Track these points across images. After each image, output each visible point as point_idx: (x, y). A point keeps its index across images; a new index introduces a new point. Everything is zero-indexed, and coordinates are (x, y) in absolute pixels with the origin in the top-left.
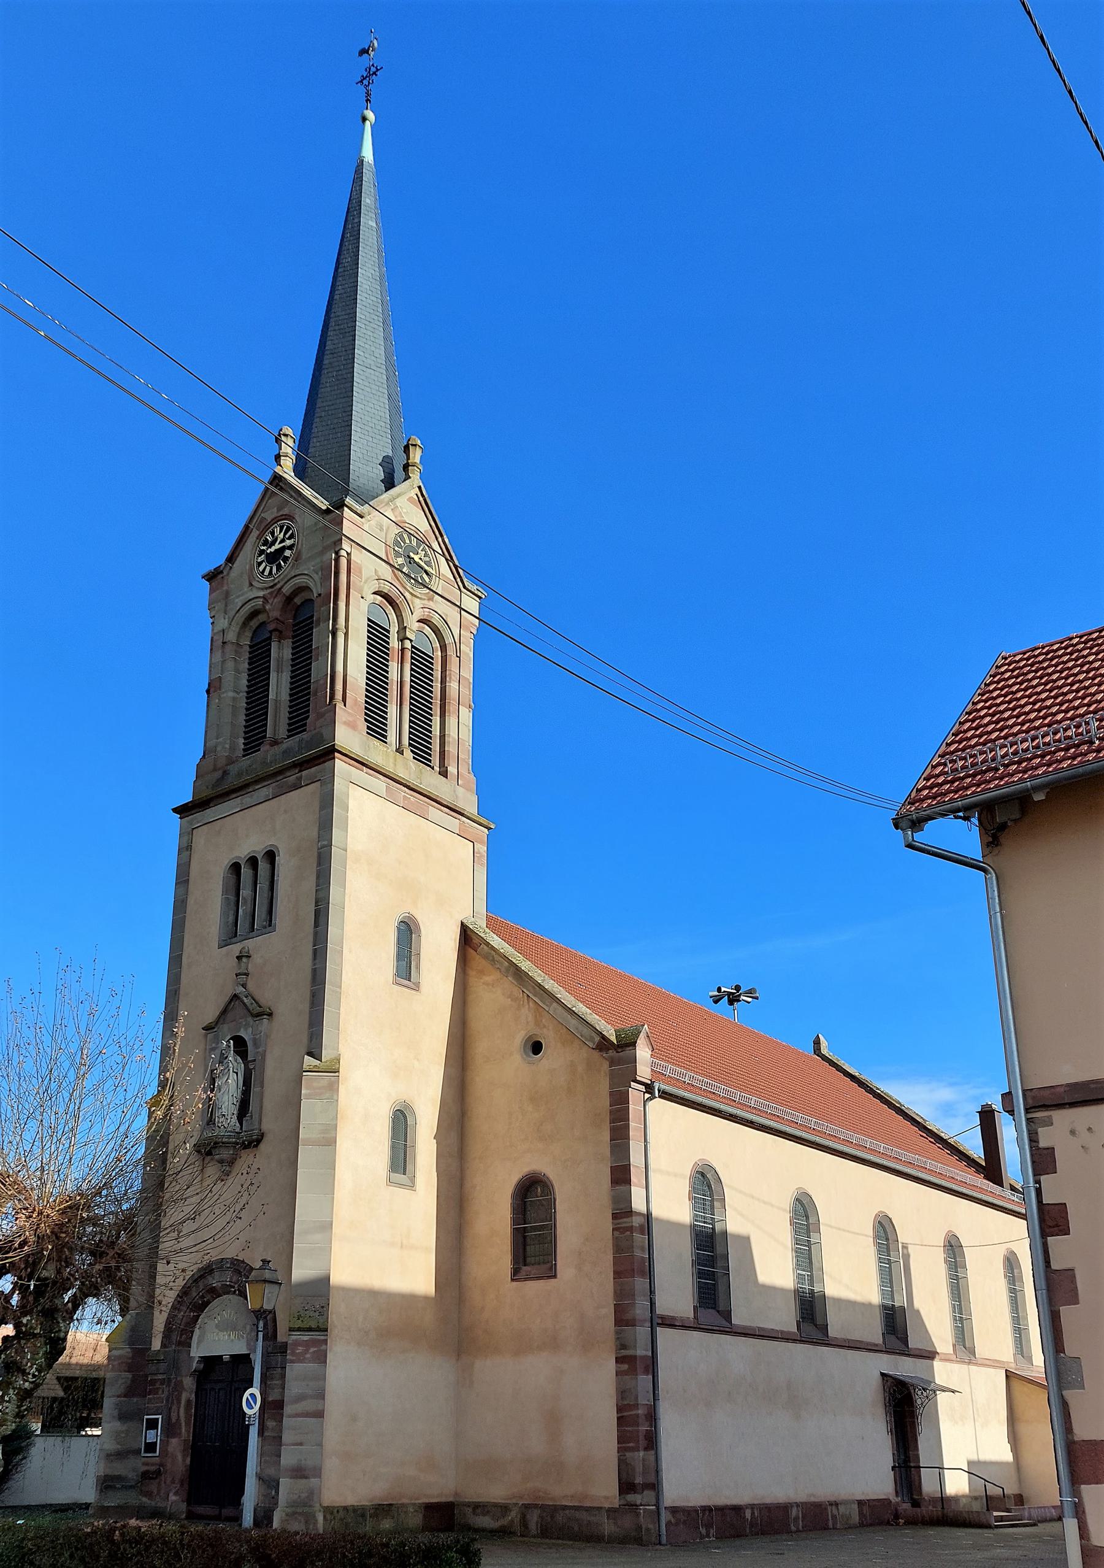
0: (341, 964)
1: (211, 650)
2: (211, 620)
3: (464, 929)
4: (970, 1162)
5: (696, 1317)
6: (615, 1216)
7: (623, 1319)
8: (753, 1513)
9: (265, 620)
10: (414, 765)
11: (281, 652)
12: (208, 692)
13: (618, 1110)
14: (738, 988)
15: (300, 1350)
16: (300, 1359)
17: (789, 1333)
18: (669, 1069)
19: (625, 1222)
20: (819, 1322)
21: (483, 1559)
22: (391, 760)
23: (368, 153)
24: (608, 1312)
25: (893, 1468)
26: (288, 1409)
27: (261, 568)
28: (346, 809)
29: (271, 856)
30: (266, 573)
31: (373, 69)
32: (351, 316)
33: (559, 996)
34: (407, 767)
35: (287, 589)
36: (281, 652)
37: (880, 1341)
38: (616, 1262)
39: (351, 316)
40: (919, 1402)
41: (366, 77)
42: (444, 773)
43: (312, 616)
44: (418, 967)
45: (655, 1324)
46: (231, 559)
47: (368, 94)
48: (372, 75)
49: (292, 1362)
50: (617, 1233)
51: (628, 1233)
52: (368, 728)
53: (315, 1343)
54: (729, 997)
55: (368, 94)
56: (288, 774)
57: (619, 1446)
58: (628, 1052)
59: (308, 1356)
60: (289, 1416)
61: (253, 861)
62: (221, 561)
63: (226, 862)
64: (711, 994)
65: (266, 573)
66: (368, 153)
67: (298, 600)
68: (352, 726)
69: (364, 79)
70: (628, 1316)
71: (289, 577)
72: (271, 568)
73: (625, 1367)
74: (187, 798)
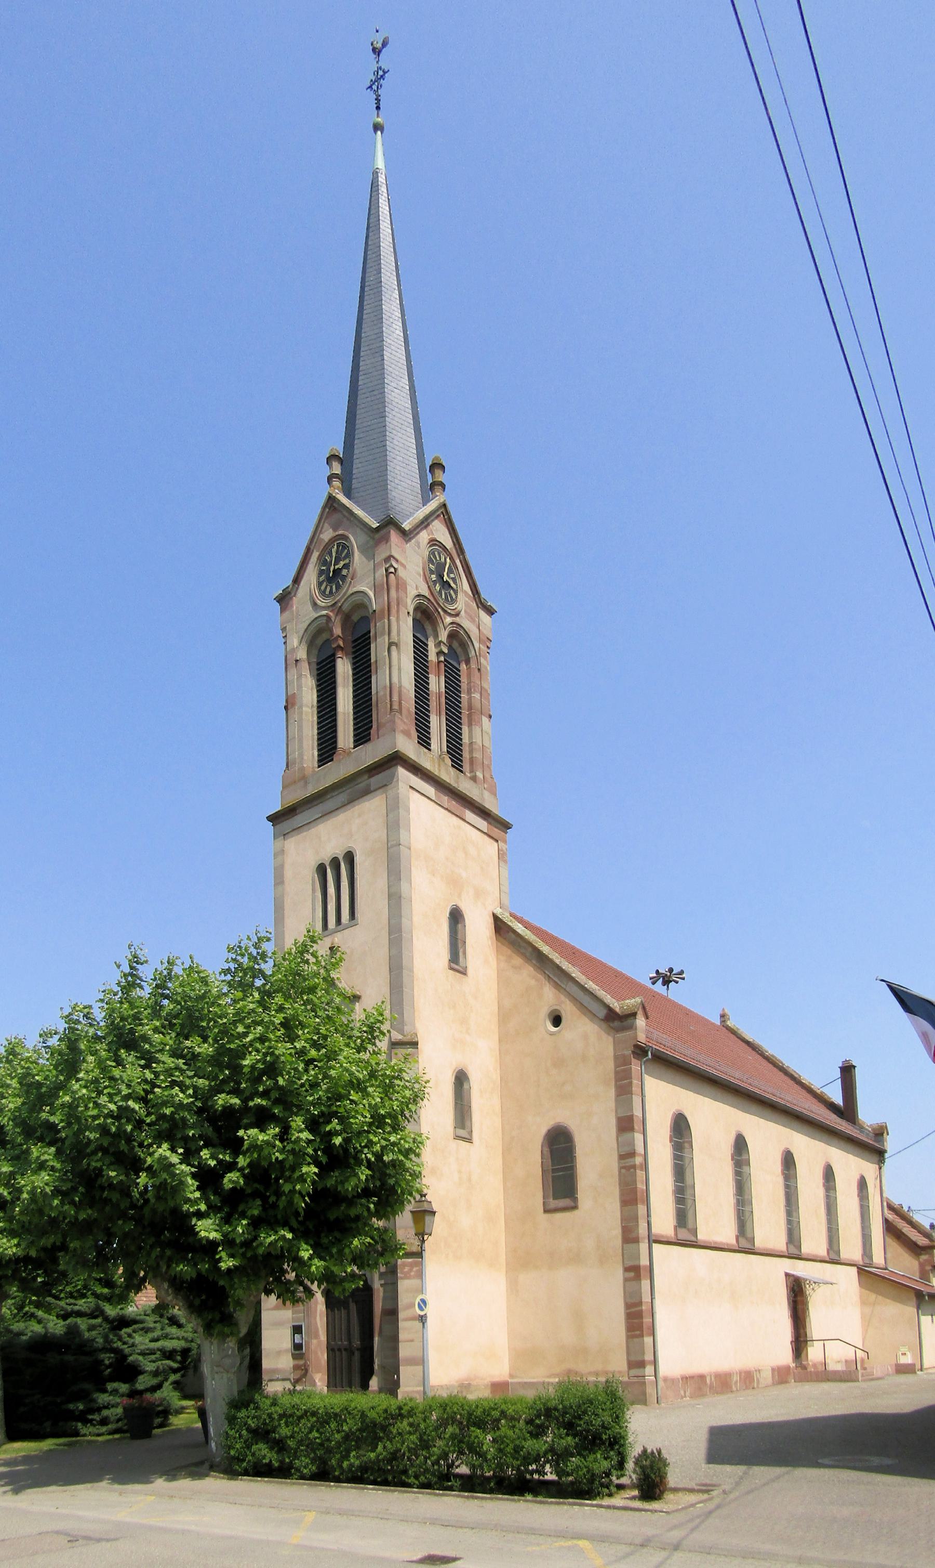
0: (412, 951)
1: (286, 668)
2: (284, 640)
3: (496, 918)
4: (832, 1107)
5: (676, 1234)
6: (622, 1157)
7: (629, 1237)
8: (711, 1379)
9: (329, 637)
10: (453, 771)
11: (344, 668)
12: (286, 708)
13: (624, 1071)
14: (671, 970)
15: (406, 1269)
16: (407, 1277)
17: (879, 1264)
18: (656, 1034)
19: (629, 1162)
20: (749, 1235)
21: (464, 1394)
22: (437, 766)
23: (380, 163)
24: (617, 1232)
25: (791, 1342)
26: (401, 1315)
27: (323, 588)
28: (408, 811)
29: (350, 857)
30: (327, 592)
31: (381, 73)
32: (378, 335)
33: (573, 975)
34: (447, 774)
35: (346, 607)
36: (344, 668)
37: (734, 1242)
38: (622, 1194)
39: (378, 335)
40: (808, 1293)
41: (375, 81)
42: (474, 779)
43: (369, 632)
44: (465, 953)
45: (651, 1241)
46: (297, 580)
47: (378, 100)
48: (380, 79)
49: (402, 1278)
50: (623, 1171)
51: (632, 1170)
52: (419, 737)
53: (416, 1264)
54: (663, 979)
55: (378, 100)
56: (359, 780)
57: (630, 1334)
58: (629, 1021)
59: (412, 1274)
60: (406, 1320)
61: (335, 863)
62: (289, 582)
63: (313, 864)
64: (651, 975)
65: (327, 592)
66: (380, 163)
67: (355, 618)
68: (407, 733)
69: (382, 76)
70: (633, 1235)
71: (347, 595)
72: (331, 587)
73: (632, 1274)
74: (277, 807)
